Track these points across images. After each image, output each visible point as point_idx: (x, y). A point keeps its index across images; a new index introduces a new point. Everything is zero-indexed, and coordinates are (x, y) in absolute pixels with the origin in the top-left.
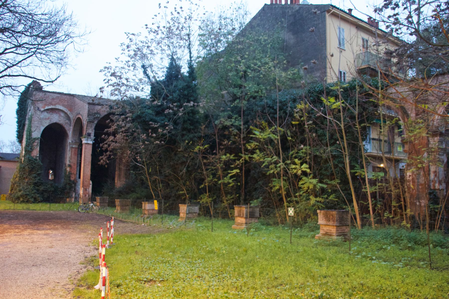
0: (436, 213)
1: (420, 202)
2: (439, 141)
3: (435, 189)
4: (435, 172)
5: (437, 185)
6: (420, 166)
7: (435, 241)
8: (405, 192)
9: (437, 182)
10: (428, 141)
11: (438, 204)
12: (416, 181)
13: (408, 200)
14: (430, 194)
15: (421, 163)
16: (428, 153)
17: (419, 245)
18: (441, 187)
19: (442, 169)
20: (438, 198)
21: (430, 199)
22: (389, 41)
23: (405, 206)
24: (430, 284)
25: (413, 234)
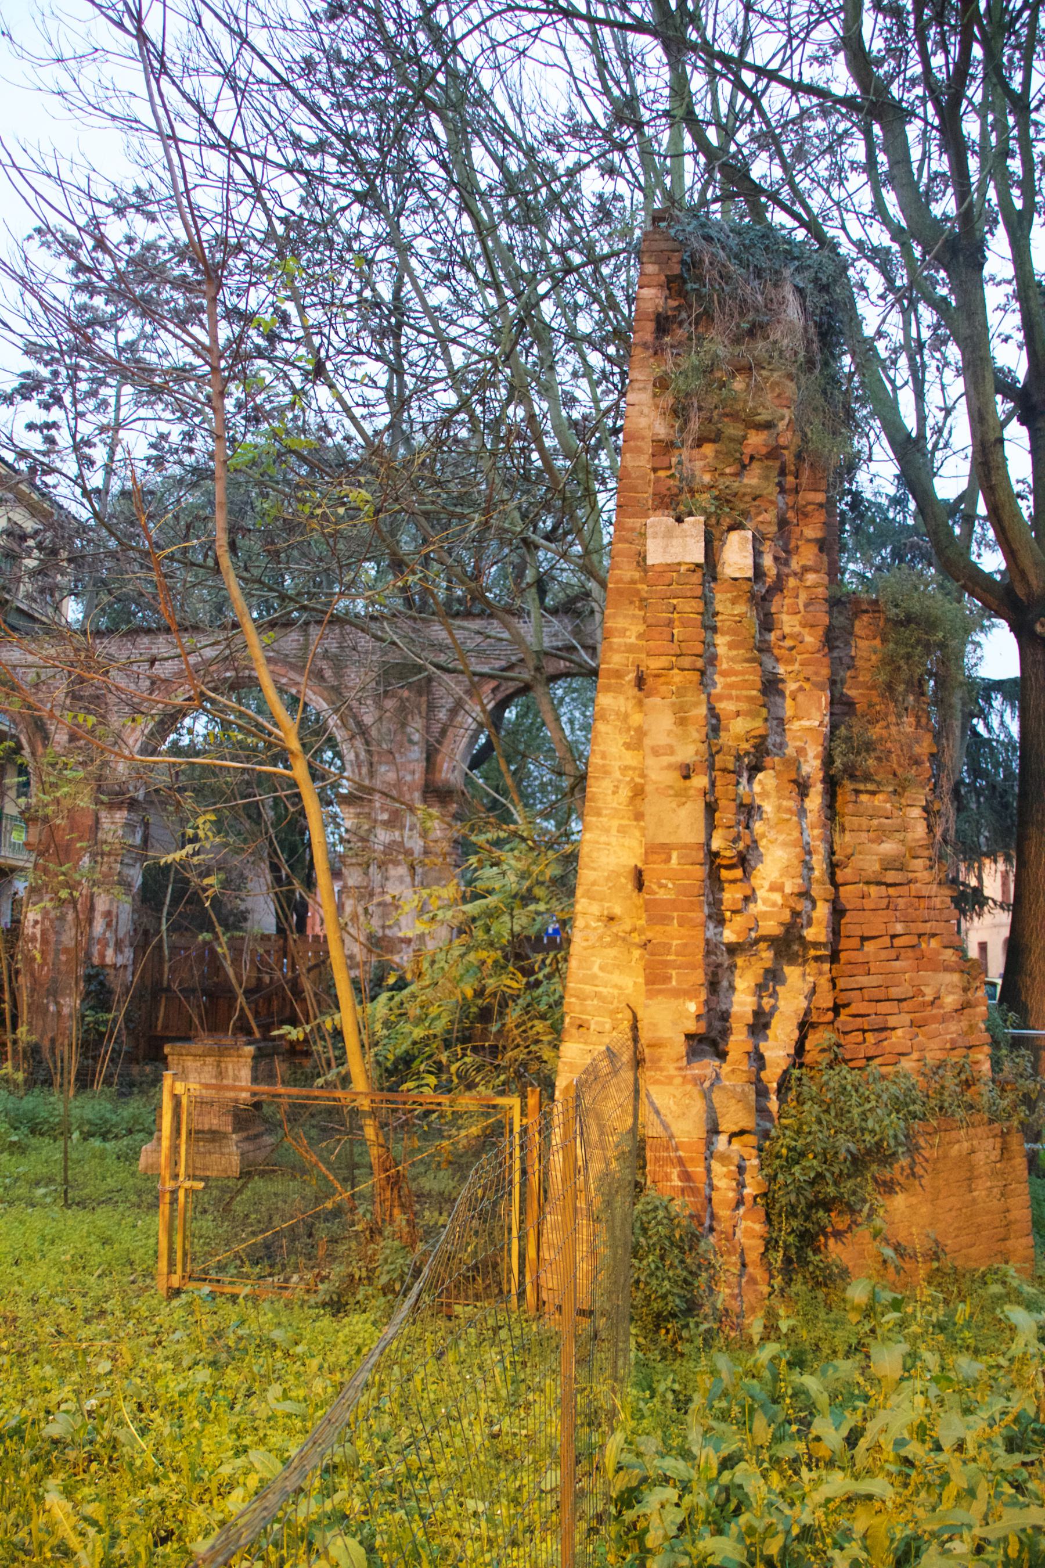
0: (102, 1035)
1: (57, 1003)
2: (126, 825)
3: (104, 966)
4: (108, 914)
5: (110, 952)
6: (64, 894)
7: (90, 1122)
8: (17, 972)
9: (112, 944)
10: (97, 820)
11: (108, 1010)
12: (52, 938)
13: (24, 998)
14: (89, 979)
15: (71, 886)
16: (93, 856)
17: (42, 1135)
18: (120, 960)
19: (128, 907)
20: (111, 992)
21: (88, 994)
22: (21, 500)
23: (15, 1018)
24: (53, 1253)
25: (29, 1103)
